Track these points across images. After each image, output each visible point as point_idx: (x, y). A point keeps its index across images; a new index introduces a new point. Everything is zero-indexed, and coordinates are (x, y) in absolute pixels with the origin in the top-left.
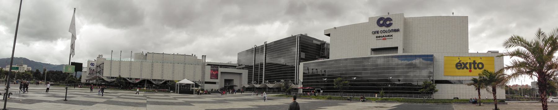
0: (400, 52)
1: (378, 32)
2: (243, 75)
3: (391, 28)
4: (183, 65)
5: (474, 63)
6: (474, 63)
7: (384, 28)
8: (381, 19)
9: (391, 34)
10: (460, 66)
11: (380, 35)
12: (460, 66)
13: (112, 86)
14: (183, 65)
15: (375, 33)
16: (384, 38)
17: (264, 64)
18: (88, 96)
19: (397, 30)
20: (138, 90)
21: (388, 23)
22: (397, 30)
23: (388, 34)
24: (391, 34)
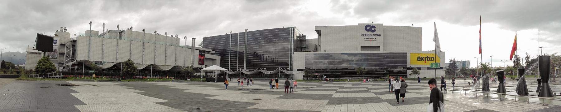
0: (382, 51)
1: (366, 35)
2: (217, 61)
3: (375, 33)
4: (175, 47)
5: (428, 57)
6: (428, 57)
7: (370, 33)
8: (368, 26)
9: (375, 37)
10: (420, 59)
11: (367, 37)
12: (420, 59)
13: (105, 75)
14: (175, 47)
15: (363, 35)
16: (371, 40)
17: (245, 53)
18: (308, 89)
19: (379, 35)
20: (168, 77)
21: (373, 29)
22: (379, 35)
23: (373, 37)
24: (375, 37)
